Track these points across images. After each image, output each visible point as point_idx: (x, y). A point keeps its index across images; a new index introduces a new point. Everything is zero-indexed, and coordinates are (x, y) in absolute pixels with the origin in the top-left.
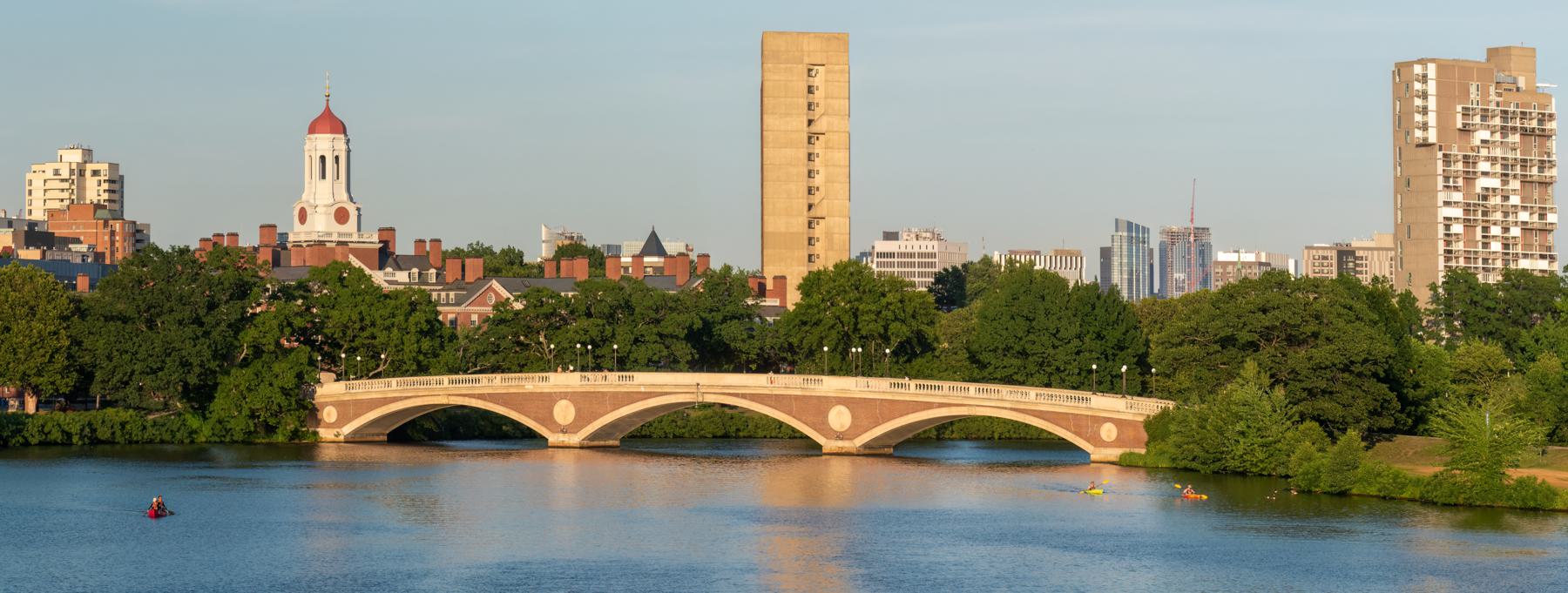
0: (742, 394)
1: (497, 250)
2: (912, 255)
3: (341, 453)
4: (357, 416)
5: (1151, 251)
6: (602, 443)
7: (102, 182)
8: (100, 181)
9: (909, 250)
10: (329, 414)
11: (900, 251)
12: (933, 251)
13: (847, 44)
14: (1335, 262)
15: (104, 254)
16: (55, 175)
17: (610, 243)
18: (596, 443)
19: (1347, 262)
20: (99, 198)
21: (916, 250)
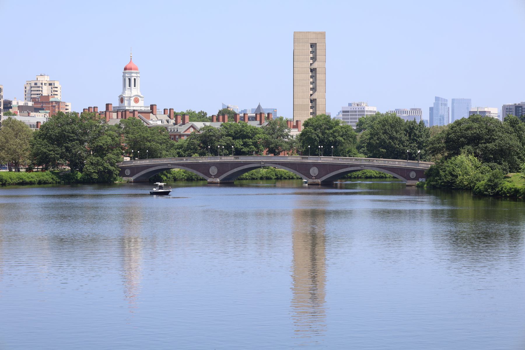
0: (279, 163)
1: (197, 112)
2: (355, 111)
3: (494, 209)
4: (137, 173)
5: (449, 108)
6: (228, 181)
7: (53, 88)
8: (52, 87)
9: (355, 110)
10: (127, 173)
11: (351, 110)
12: (356, 110)
13: (325, 35)
14: (514, 110)
15: (311, 109)
16: (35, 85)
17: (518, 102)
18: (225, 181)
19: (519, 110)
20: (52, 93)
21: (357, 109)
